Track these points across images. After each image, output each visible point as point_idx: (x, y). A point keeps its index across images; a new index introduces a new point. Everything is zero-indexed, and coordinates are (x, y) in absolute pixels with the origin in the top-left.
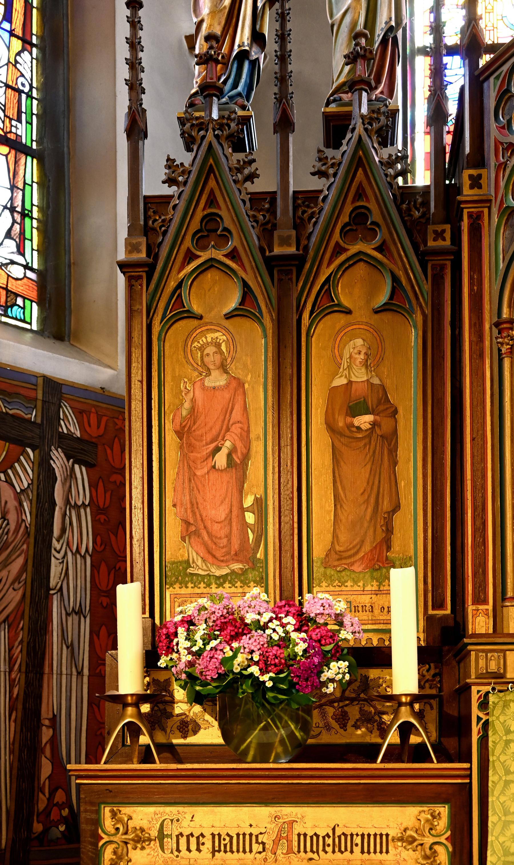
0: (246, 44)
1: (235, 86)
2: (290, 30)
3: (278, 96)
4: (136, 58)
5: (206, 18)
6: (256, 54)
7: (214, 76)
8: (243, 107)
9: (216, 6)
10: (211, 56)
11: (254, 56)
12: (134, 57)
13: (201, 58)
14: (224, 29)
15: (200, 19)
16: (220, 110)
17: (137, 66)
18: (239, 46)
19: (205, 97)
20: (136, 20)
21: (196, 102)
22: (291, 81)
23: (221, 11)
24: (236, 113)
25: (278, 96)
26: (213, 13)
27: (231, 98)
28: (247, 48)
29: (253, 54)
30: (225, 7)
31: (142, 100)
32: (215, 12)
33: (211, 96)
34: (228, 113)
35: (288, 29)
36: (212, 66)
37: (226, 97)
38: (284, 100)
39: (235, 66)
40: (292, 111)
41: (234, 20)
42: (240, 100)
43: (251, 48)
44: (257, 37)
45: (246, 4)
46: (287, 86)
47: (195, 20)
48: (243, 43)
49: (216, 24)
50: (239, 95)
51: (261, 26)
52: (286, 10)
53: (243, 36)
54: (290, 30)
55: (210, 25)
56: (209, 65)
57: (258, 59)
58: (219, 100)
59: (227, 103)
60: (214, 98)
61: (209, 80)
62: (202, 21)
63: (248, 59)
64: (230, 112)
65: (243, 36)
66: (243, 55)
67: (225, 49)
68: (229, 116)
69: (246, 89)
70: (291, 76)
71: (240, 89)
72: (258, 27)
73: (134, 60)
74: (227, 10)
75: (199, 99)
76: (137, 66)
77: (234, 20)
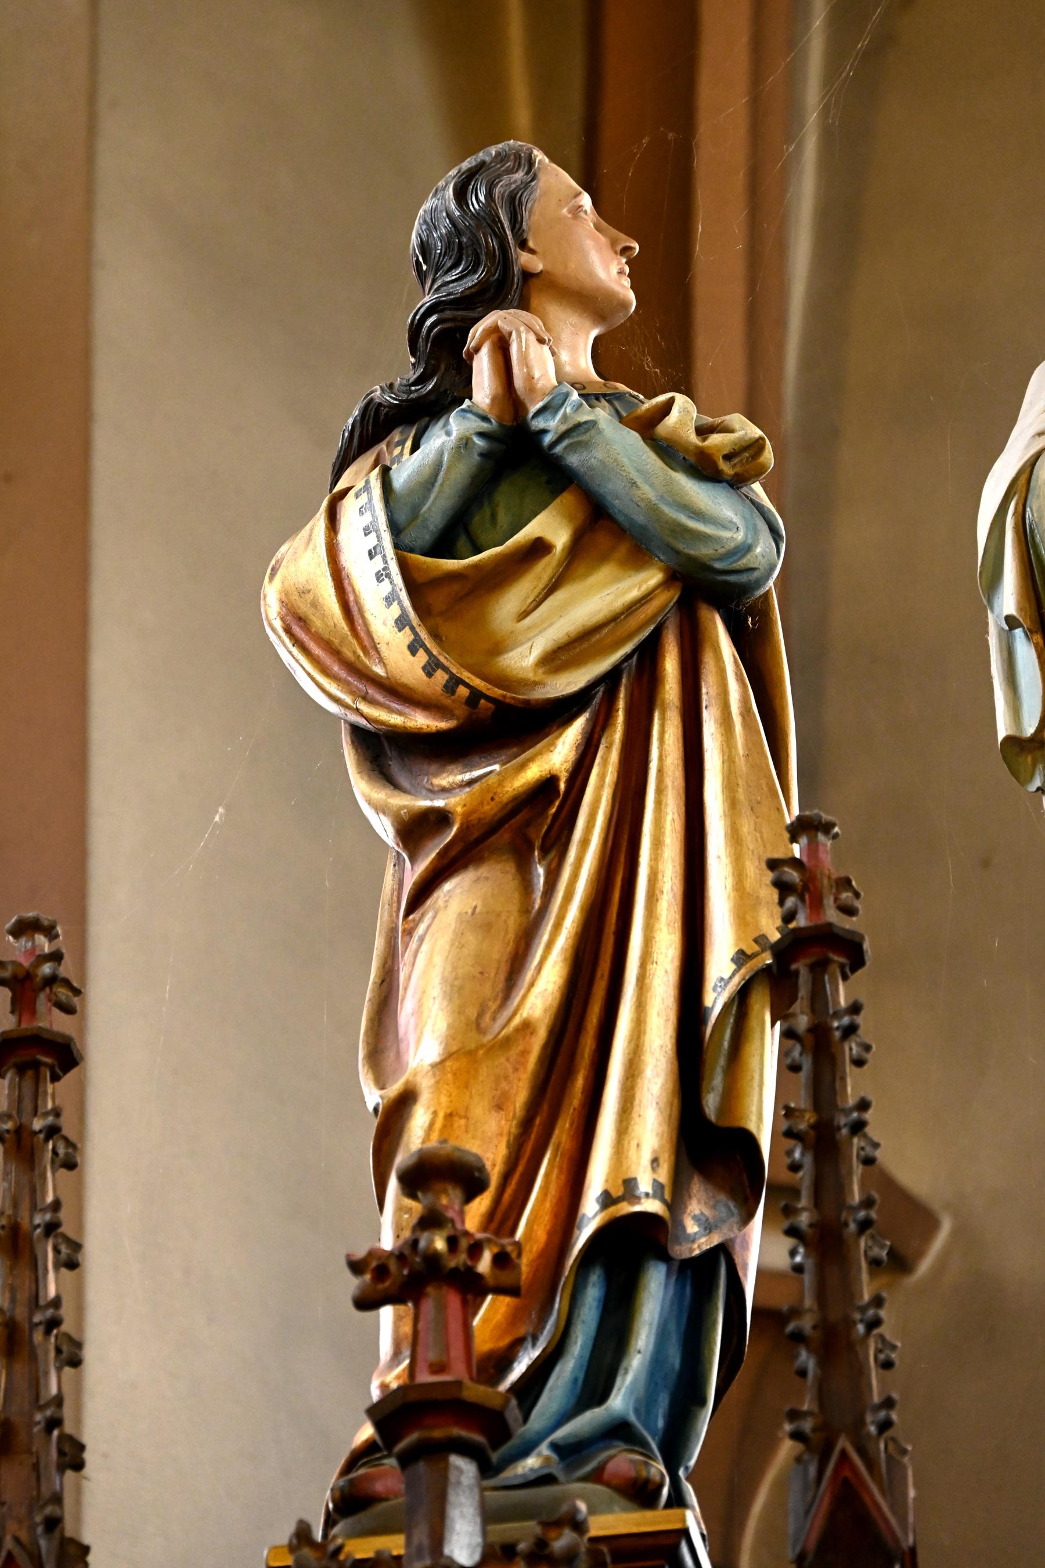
0: (645, 1185)
1: (595, 1387)
2: (863, 1105)
3: (807, 1425)
4: (35, 1302)
5: (425, 1086)
6: (708, 1228)
7: (457, 1352)
8: (641, 1494)
9: (478, 1025)
10: (433, 1259)
11: (696, 1235)
12: (23, 1295)
13: (381, 1272)
14: (526, 1124)
15: (394, 1089)
16: (489, 1516)
17: (38, 1336)
18: (607, 1200)
19: (406, 1460)
20: (37, 1124)
21: (379, 1487)
22: (886, 1344)
23: (506, 1043)
24: (579, 1526)
25: (807, 1425)
26: (462, 1058)
27: (570, 1452)
28: (652, 1206)
29: (692, 1228)
30: (527, 1027)
31: (57, 1499)
32: (471, 1054)
33: (437, 1451)
34: (532, 1527)
35: (851, 1101)
36: (442, 1308)
37: (544, 1449)
38: (843, 1443)
39: (593, 1294)
40: (894, 1488)
41: (580, 1082)
42: (622, 1461)
43: (676, 1201)
44: (707, 1146)
45: (641, 1006)
46: (860, 1373)
47: (373, 1097)
48: (630, 1185)
49: (480, 1109)
50: (620, 1431)
51: (732, 1095)
52: (837, 1015)
53: (632, 1147)
54: (863, 1105)
55: (449, 1116)
56: (428, 1306)
57: (723, 1255)
58: (487, 1469)
59: (545, 1479)
60: (457, 1461)
61: (424, 1377)
62: (406, 1100)
63: (664, 1256)
64: (546, 1525)
65: (632, 1147)
66: (631, 1243)
67: (531, 1225)
68: (541, 1543)
69: (663, 1401)
70: (876, 1323)
71: (619, 1402)
72: (711, 1103)
73: (21, 1313)
74: (541, 1035)
75: (387, 1477)
76: (38, 1336)
77: (580, 1082)
